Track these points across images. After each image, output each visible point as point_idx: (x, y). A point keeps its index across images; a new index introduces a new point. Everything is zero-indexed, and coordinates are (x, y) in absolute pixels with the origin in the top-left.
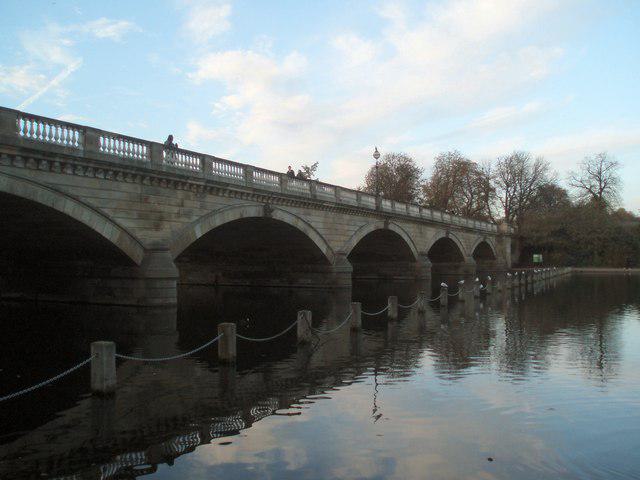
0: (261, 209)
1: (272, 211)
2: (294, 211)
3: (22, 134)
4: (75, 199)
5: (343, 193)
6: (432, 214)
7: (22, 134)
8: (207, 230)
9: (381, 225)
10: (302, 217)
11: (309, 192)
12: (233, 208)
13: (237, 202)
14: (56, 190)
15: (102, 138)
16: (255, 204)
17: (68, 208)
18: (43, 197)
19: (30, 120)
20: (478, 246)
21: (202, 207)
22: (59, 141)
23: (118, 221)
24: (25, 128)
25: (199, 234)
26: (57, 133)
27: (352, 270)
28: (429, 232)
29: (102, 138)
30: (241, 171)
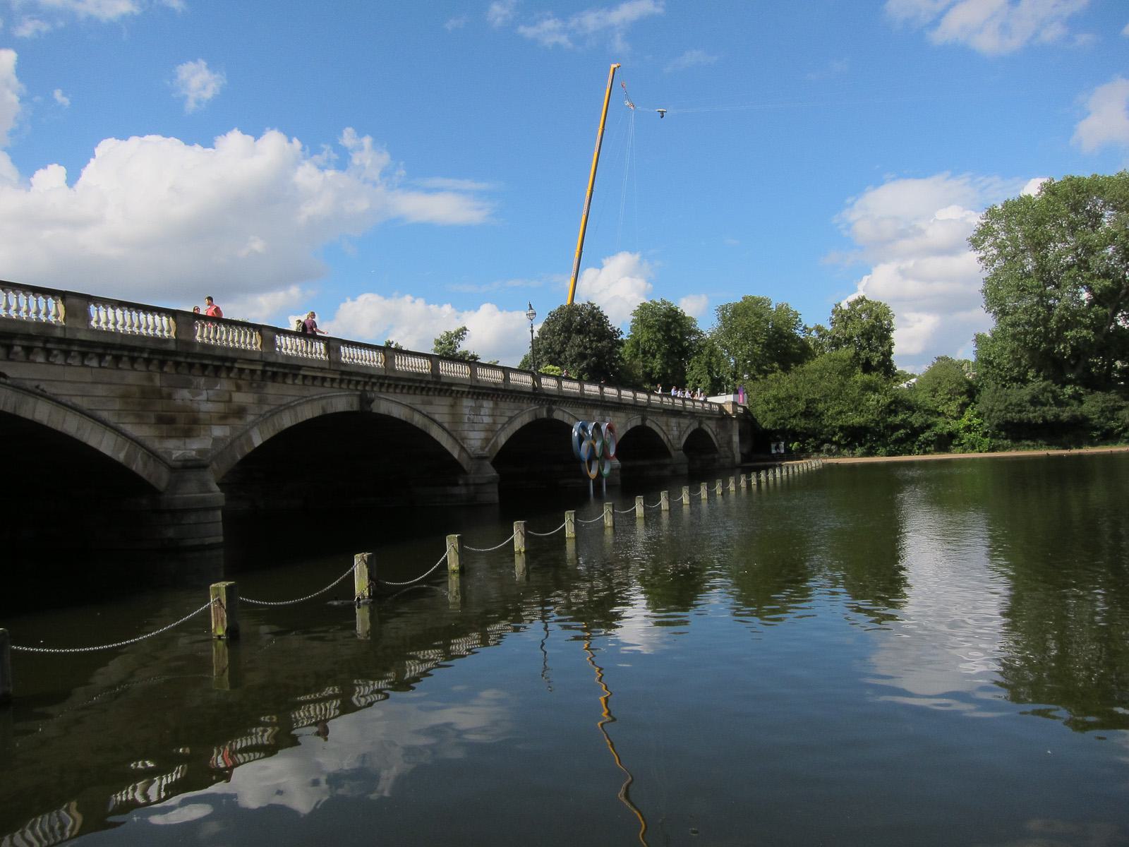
21: (261, 401)
25: (258, 441)
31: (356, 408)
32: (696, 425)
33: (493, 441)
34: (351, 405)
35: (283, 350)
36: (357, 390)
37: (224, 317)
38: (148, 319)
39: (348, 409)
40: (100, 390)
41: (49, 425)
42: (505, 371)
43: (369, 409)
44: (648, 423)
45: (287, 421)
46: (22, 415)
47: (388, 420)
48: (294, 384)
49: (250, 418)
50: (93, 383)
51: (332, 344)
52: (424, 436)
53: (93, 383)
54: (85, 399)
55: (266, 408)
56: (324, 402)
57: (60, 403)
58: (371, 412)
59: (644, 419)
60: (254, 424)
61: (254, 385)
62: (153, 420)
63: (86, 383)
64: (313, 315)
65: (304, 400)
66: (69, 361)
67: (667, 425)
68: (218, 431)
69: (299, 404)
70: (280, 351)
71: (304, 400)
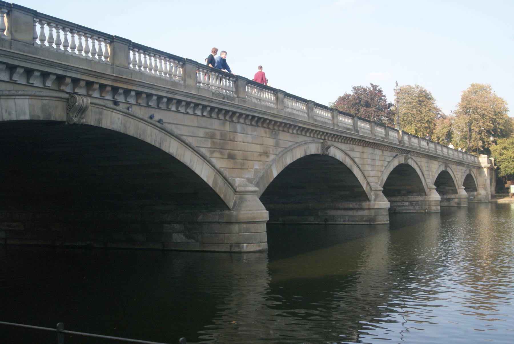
0: (320, 145)
1: (329, 147)
2: (343, 147)
3: (38, 42)
4: (178, 138)
5: (318, 111)
6: (419, 143)
7: (38, 42)
8: (280, 170)
9: (314, 149)
10: (349, 153)
11: (418, 145)
12: (299, 144)
13: (302, 139)
14: (160, 125)
15: (38, 26)
16: (316, 140)
17: (172, 148)
18: (151, 136)
19: (49, 24)
20: (392, 173)
21: (277, 145)
22: (76, 51)
23: (214, 161)
24: (51, 37)
25: (275, 174)
26: (58, 36)
27: (440, 199)
28: (433, 166)
29: (38, 26)
30: (105, 48)
31: (320, 152)
32: (442, 168)
33: (381, 178)
34: (318, 149)
35: (69, 49)
36: (321, 139)
37: (269, 84)
38: (45, 30)
39: (317, 153)
40: (201, 133)
41: (177, 158)
42: (240, 82)
43: (327, 153)
44: (411, 162)
45: (289, 160)
46: (164, 149)
47: (334, 159)
48: (178, 111)
49: (272, 157)
50: (198, 127)
51: (280, 96)
52: (350, 172)
53: (198, 127)
54: (194, 138)
55: (279, 150)
56: (305, 147)
57: (183, 142)
58: (327, 156)
59: (406, 159)
60: (274, 160)
61: (274, 133)
62: (226, 157)
63: (194, 127)
64: (261, 67)
65: (298, 145)
66: (90, 93)
67: (361, 158)
68: (257, 166)
69: (295, 148)
70: (66, 50)
71: (298, 145)
